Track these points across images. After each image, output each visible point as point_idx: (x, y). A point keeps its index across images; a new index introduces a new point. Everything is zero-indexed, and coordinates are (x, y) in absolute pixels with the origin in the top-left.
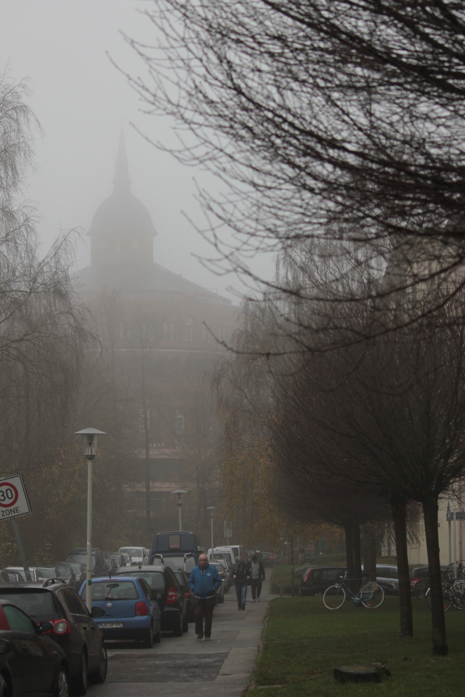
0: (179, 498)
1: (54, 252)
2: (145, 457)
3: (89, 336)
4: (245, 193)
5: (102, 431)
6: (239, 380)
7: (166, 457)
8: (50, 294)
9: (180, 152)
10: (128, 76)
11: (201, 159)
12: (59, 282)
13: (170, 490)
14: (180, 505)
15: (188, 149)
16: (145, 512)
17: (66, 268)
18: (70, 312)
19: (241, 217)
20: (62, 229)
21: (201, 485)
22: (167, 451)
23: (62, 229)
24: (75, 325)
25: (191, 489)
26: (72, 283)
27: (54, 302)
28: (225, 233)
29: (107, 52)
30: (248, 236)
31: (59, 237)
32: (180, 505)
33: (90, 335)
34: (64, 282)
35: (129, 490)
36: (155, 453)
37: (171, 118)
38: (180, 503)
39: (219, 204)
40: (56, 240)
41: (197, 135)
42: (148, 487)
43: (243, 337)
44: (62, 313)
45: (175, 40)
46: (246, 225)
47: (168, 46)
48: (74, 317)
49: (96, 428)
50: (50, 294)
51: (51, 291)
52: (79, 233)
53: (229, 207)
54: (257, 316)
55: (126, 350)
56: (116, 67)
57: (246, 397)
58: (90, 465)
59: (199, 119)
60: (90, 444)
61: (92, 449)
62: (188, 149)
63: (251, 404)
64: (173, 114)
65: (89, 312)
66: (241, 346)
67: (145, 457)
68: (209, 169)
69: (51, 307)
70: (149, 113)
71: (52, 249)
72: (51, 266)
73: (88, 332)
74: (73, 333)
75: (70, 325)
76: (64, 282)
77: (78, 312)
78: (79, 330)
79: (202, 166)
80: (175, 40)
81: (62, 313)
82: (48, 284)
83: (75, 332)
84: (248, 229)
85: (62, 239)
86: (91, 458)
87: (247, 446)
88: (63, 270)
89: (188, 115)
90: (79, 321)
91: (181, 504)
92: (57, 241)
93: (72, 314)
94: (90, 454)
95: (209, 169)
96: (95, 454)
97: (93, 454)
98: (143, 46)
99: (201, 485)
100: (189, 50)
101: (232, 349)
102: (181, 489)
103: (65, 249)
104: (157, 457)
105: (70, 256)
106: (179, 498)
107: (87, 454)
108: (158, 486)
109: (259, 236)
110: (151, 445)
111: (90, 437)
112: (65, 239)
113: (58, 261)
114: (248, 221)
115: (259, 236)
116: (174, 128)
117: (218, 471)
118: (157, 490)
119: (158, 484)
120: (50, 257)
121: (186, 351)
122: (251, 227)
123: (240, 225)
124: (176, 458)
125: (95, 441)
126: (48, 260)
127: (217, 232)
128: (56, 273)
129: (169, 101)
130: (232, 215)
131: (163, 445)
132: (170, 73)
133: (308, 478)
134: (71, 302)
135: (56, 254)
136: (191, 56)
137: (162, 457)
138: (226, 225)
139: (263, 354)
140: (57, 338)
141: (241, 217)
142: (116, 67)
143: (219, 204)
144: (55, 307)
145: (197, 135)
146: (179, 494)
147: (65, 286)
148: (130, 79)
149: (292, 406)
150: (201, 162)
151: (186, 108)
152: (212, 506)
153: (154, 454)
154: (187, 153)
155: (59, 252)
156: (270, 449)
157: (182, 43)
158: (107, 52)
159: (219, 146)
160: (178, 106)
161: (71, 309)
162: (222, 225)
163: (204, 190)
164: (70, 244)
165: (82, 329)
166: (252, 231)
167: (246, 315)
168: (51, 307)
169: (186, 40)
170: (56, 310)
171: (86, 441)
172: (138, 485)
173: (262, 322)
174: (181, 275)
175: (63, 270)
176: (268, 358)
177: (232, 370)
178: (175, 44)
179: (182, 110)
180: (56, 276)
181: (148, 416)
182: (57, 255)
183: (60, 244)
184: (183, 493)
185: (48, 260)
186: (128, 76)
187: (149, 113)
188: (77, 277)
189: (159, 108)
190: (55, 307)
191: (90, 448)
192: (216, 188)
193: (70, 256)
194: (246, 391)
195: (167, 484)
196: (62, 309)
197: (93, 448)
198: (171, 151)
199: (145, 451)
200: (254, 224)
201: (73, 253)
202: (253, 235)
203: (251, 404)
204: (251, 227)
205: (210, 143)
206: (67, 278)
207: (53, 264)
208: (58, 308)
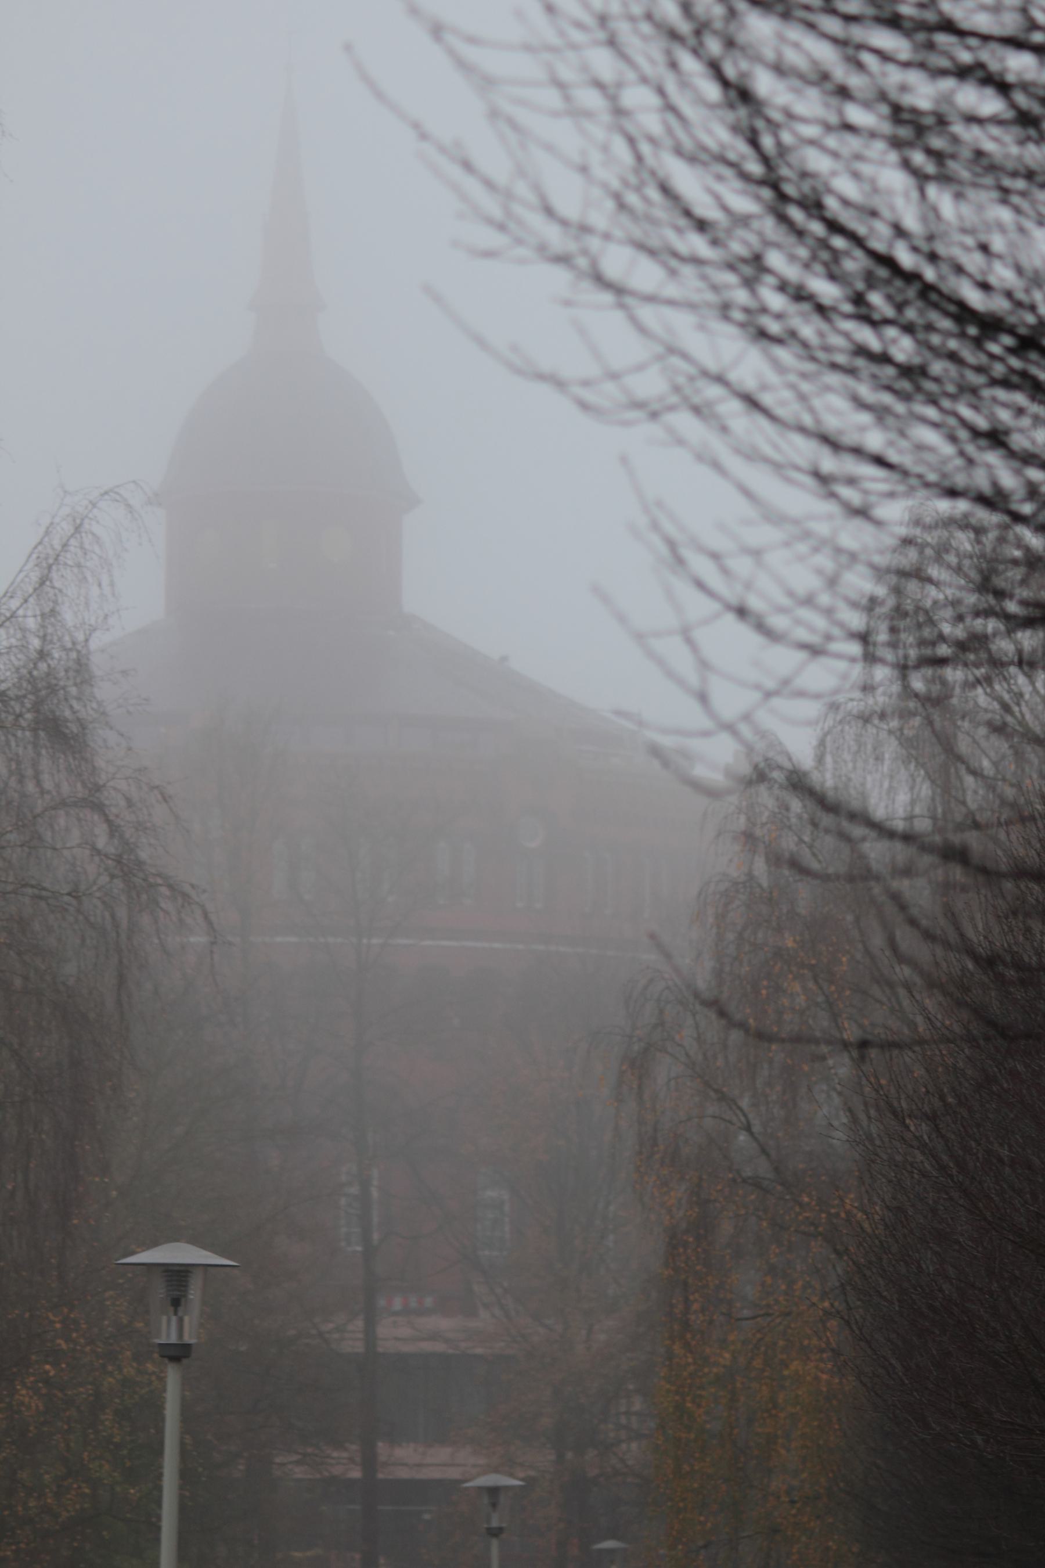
0: (494, 1505)
1: (35, 577)
2: (359, 1347)
3: (164, 890)
4: (796, 522)
5: (222, 1254)
6: (720, 1062)
7: (439, 1347)
8: (19, 733)
9: (586, 383)
10: (416, 126)
11: (655, 406)
12: (52, 689)
13: (453, 1474)
14: (495, 1533)
15: (614, 376)
16: (357, 1556)
17: (80, 637)
18: (93, 801)
19: (785, 601)
20: (65, 492)
21: (569, 1455)
22: (443, 1324)
23: (65, 492)
24: (112, 850)
25: (532, 1473)
26: (104, 692)
27: (35, 764)
28: (731, 643)
29: (348, 48)
30: (802, 655)
31: (57, 520)
32: (495, 1533)
33: (170, 887)
34: (73, 690)
35: (299, 1472)
36: (407, 1329)
37: (561, 276)
38: (495, 1523)
39: (715, 556)
40: (42, 530)
41: (642, 329)
42: (370, 1462)
43: (737, 903)
44: (64, 804)
45: (579, 25)
46: (798, 622)
47: (555, 40)
48: (108, 821)
49: (196, 1241)
50: (19, 733)
51: (24, 724)
52: (128, 506)
53: (742, 566)
54: (790, 828)
55: (293, 939)
56: (380, 95)
57: (748, 1128)
58: (173, 1376)
59: (646, 275)
60: (176, 1303)
61: (181, 1321)
62: (614, 376)
63: (768, 1155)
64: (563, 259)
65: (165, 799)
66: (731, 936)
67: (359, 1347)
68: (680, 442)
69: (21, 780)
70: (489, 254)
71: (30, 565)
72: (23, 630)
73: (159, 875)
74: (104, 879)
75: (96, 851)
76: (73, 690)
77: (123, 803)
78: (126, 867)
79: (654, 429)
80: (579, 25)
81: (64, 804)
82: (11, 693)
83: (112, 876)
84: (802, 634)
85: (67, 528)
86: (178, 1354)
87: (746, 1313)
88: (69, 645)
89: (618, 261)
90: (127, 835)
91: (500, 1530)
92: (47, 533)
93: (99, 808)
94: (173, 1339)
95: (680, 442)
96: (193, 1341)
97: (187, 1339)
98: (473, 40)
99: (569, 1455)
100: (623, 56)
101: (742, 1025)
102: (496, 1470)
103: (79, 566)
104: (407, 1348)
105: (95, 591)
106: (494, 1505)
107: (163, 1341)
108: (409, 1460)
109: (839, 656)
110: (382, 1302)
111: (177, 1276)
112: (78, 529)
113: (52, 611)
114: (805, 613)
115: (839, 656)
116: (568, 303)
117: (638, 1405)
118: (403, 1474)
119: (406, 1452)
120: (19, 593)
121: (521, 947)
122: (812, 629)
123: (778, 622)
124: (479, 1351)
125: (195, 1293)
126: (14, 604)
127: (700, 635)
128: (42, 655)
129: (549, 211)
130: (748, 586)
131: (429, 1301)
132: (564, 134)
133: (979, 1439)
134: (100, 763)
135: (42, 583)
136: (631, 76)
137: (427, 1346)
138: (730, 618)
139: (846, 1045)
140: (41, 898)
141: (785, 601)
142: (380, 95)
143: (715, 556)
144: (39, 783)
145: (642, 329)
146: (494, 1492)
147: (75, 703)
148: (424, 136)
149: (924, 1174)
150: (654, 415)
151: (607, 237)
152: (614, 1537)
153: (396, 1334)
154: (610, 387)
155: (54, 575)
156: (833, 1324)
157: (601, 35)
158: (348, 48)
159: (712, 366)
160: (585, 229)
161: (98, 788)
162: (717, 616)
163: (659, 504)
164: (97, 549)
165: (140, 863)
166: (814, 639)
167: (748, 819)
168: (21, 780)
169: (613, 25)
170: (43, 792)
171: (159, 1291)
172: (335, 1454)
173: (811, 847)
174: (504, 659)
175: (69, 645)
176: (862, 1058)
177: (697, 1026)
178: (577, 36)
179: (594, 243)
180: (43, 666)
181: (375, 1193)
182: (47, 588)
183: (58, 547)
184: (507, 1488)
185: (14, 604)
186: (416, 126)
187: (489, 254)
188: (124, 673)
189: (519, 241)
190: (39, 783)
191: (174, 1319)
192: (706, 506)
193: (95, 591)
194: (745, 1103)
195: (443, 1453)
196: (65, 789)
197: (186, 1319)
198: (559, 383)
199: (359, 1323)
200: (821, 623)
201: (105, 581)
202: (815, 651)
203: (768, 1155)
204: (812, 629)
205: (685, 356)
206: (81, 669)
207: (31, 623)
208: (48, 785)
